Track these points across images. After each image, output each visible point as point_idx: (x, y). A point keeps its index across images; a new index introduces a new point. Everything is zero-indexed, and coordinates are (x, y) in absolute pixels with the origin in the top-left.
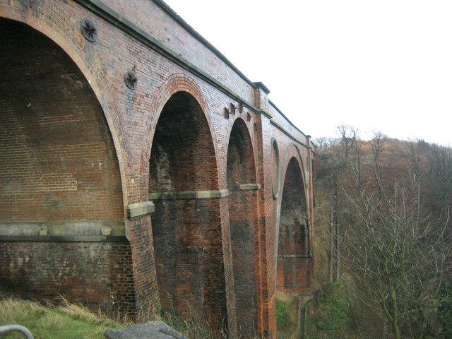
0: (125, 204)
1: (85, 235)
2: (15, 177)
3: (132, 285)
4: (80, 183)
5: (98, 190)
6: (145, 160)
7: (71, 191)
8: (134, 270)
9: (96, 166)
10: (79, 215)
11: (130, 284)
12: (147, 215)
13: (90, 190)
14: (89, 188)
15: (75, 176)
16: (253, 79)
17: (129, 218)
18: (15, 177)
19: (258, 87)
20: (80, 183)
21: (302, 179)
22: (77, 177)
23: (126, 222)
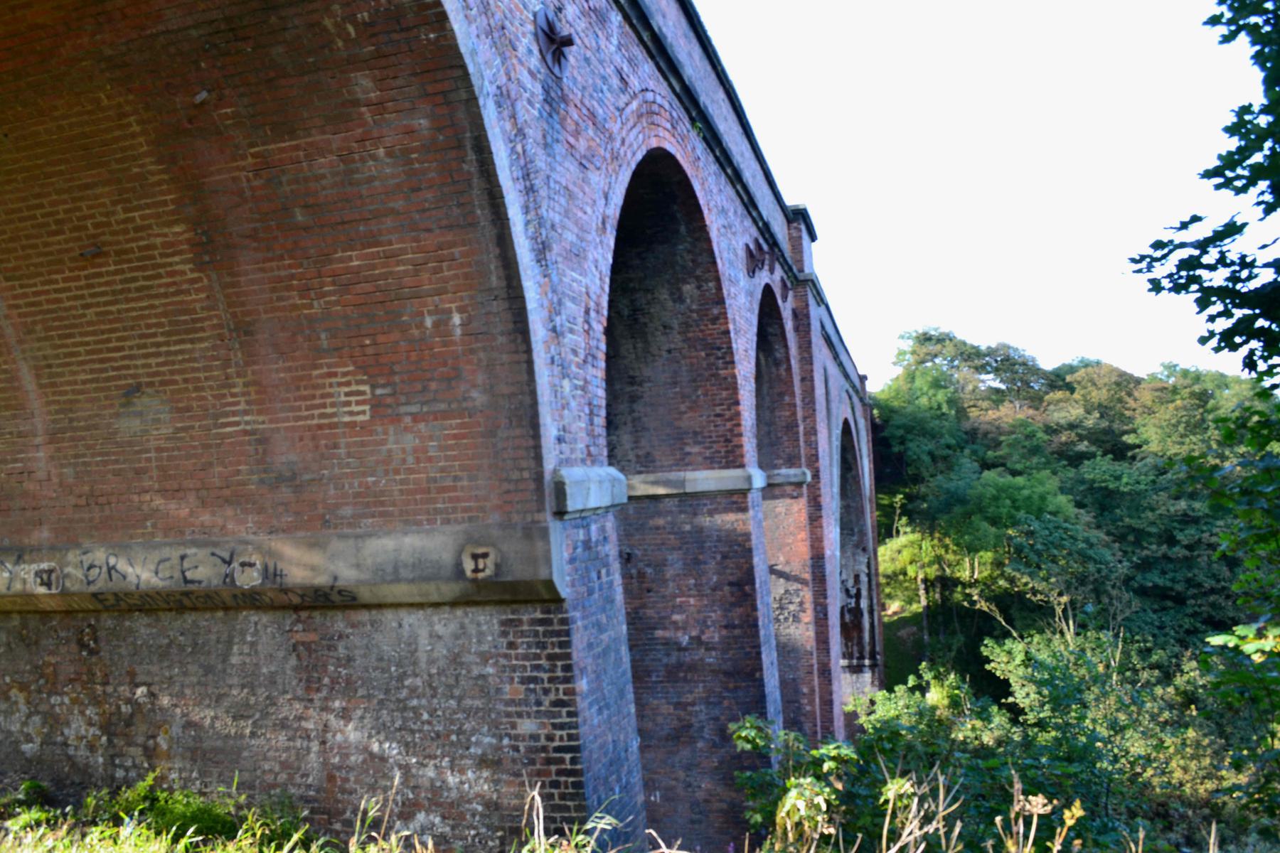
0: (549, 464)
1: (397, 580)
2: (151, 384)
3: (574, 761)
4: (379, 392)
5: (446, 415)
6: (594, 324)
7: (347, 424)
8: (582, 704)
9: (442, 324)
10: (172, 200)
11: (568, 756)
12: (607, 509)
13: (416, 418)
14: (414, 409)
15: (362, 368)
16: (790, 200)
17: (560, 513)
18: (151, 384)
19: (798, 217)
20: (379, 392)
21: (853, 446)
22: (373, 368)
23: (555, 527)
